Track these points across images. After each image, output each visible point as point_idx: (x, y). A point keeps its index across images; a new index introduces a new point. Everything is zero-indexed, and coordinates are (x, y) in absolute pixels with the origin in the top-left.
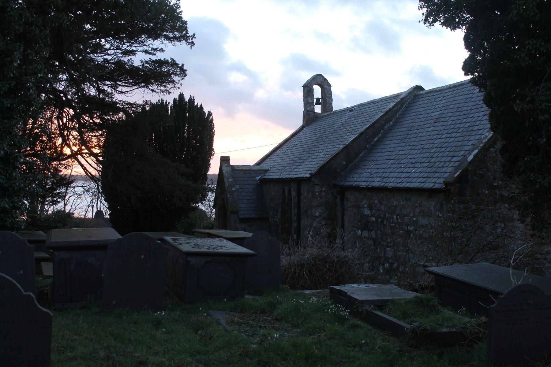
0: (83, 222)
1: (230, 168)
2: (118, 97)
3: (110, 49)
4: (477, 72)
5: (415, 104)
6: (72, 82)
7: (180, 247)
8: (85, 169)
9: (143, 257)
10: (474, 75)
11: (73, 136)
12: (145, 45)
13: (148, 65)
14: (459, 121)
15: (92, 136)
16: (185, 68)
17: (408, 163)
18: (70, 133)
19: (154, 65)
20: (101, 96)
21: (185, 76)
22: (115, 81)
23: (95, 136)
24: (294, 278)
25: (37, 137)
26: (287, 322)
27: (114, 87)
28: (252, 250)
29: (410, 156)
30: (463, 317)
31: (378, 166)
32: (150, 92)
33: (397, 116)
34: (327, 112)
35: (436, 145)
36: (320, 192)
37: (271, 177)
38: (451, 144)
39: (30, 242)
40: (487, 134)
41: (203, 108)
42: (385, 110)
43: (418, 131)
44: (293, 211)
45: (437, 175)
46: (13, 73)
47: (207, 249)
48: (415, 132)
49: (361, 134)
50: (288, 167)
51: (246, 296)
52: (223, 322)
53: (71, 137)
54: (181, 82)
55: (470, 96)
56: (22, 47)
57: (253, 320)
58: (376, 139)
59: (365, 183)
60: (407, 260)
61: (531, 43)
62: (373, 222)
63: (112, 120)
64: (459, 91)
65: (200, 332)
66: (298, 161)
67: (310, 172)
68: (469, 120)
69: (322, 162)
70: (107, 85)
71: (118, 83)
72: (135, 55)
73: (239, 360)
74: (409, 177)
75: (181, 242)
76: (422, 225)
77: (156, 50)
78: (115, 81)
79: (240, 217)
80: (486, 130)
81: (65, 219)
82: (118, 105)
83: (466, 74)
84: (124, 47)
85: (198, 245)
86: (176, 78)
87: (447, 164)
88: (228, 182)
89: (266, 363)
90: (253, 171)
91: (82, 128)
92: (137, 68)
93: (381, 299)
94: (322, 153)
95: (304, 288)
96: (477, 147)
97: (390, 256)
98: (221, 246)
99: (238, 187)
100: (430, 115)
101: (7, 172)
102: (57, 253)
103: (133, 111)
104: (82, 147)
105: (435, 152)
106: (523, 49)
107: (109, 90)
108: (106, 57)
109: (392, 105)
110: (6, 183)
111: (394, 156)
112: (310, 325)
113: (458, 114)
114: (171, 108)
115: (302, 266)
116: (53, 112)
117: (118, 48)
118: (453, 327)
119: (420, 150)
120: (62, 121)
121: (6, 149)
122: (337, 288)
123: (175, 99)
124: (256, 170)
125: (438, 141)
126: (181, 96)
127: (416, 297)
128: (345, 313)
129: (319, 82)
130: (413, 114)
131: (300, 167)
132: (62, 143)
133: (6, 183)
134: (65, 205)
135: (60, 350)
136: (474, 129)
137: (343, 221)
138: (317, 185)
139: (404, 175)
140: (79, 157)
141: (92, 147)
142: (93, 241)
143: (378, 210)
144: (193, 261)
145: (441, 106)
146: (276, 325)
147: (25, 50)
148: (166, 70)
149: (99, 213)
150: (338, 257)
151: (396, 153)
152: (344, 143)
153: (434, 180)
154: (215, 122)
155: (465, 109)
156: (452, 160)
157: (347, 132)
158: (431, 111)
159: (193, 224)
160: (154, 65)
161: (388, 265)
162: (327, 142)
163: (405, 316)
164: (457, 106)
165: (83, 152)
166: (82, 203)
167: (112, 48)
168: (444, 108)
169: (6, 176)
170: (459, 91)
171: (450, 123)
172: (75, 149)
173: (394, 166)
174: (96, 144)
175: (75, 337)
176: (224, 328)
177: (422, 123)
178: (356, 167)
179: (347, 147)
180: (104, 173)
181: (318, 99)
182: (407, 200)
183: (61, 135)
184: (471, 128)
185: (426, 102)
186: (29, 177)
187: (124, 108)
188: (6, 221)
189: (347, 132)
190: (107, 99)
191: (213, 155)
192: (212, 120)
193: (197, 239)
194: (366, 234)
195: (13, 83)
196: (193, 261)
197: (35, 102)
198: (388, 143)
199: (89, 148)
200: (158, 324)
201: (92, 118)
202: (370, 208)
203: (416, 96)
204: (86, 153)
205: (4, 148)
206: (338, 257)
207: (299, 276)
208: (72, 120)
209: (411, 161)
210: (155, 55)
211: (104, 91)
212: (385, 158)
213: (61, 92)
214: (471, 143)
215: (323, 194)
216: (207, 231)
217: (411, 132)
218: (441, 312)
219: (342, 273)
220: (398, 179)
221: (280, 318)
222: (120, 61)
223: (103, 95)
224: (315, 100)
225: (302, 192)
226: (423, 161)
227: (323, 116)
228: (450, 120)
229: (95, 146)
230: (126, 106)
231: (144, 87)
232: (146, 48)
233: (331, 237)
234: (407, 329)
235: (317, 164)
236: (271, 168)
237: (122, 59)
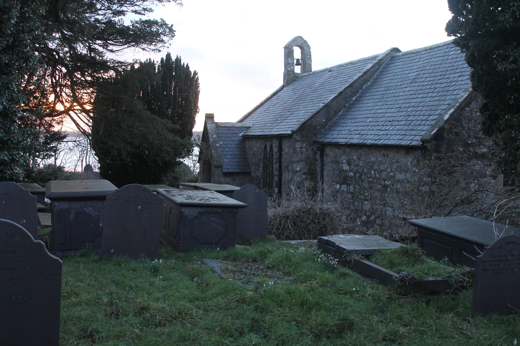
0: (72, 176)
1: (214, 125)
2: (108, 56)
3: (100, 9)
4: (459, 33)
5: (392, 65)
6: (64, 40)
8: (77, 125)
9: (140, 207)
10: (456, 36)
11: (65, 93)
12: (136, 5)
13: (138, 25)
14: (435, 82)
15: (83, 93)
16: (174, 28)
17: (386, 121)
18: (63, 90)
19: (143, 25)
20: (92, 55)
21: (173, 36)
22: (106, 40)
24: (279, 229)
25: (32, 93)
26: (278, 271)
29: (388, 115)
30: (447, 267)
31: (356, 124)
32: (141, 50)
33: (375, 76)
34: (306, 72)
35: (412, 105)
36: (301, 148)
37: (254, 134)
38: (427, 104)
39: (32, 193)
40: (462, 94)
41: (189, 68)
42: (364, 71)
43: (395, 91)
44: (274, 166)
45: (414, 133)
46: (11, 30)
47: (200, 200)
48: (392, 91)
49: (341, 93)
50: (269, 125)
51: (237, 246)
52: (218, 270)
53: (63, 94)
54: (170, 42)
55: (446, 58)
56: (19, 5)
57: (246, 268)
58: (354, 99)
59: (344, 140)
60: (383, 213)
61: (516, 4)
62: (351, 177)
63: (103, 78)
64: (435, 53)
65: (195, 279)
66: (279, 119)
67: (291, 129)
68: (444, 81)
69: (303, 119)
70: (98, 44)
72: (124, 15)
73: (237, 307)
74: (387, 135)
75: (174, 194)
76: (399, 180)
77: (145, 9)
78: (106, 40)
79: (224, 171)
80: (462, 91)
81: (56, 173)
82: (108, 64)
83: (449, 35)
85: (190, 197)
86: (165, 38)
87: (424, 122)
88: (212, 138)
89: (263, 309)
90: (235, 127)
91: (74, 85)
92: (128, 28)
93: (368, 249)
94: (303, 112)
95: (288, 238)
96: (453, 106)
97: (368, 210)
99: (221, 143)
100: (406, 75)
101: (6, 126)
102: (56, 204)
103: (123, 69)
104: (73, 103)
105: (412, 111)
106: (508, 11)
107: (101, 49)
108: (97, 17)
109: (370, 66)
110: (5, 136)
111: (372, 115)
112: (302, 273)
113: (434, 75)
114: (158, 67)
115: (287, 217)
116: (46, 70)
117: (109, 8)
118: (439, 276)
119: (398, 109)
120: (55, 79)
121: (4, 103)
122: (325, 238)
123: (162, 59)
124: (239, 127)
125: (414, 100)
126: (168, 56)
127: (402, 248)
128: (334, 262)
129: (299, 44)
130: (390, 75)
131: (282, 124)
132: (55, 100)
133: (5, 136)
134: (56, 159)
135: (65, 296)
136: (450, 89)
137: (322, 176)
138: (297, 141)
139: (382, 133)
140: (71, 113)
141: (84, 104)
142: (92, 192)
143: (357, 166)
144: (186, 211)
145: (417, 67)
146: (268, 273)
147: (22, 8)
148: (155, 30)
149: (88, 168)
150: (321, 209)
151: (373, 111)
152: (324, 102)
153: (411, 138)
155: (441, 70)
156: (428, 119)
157: (326, 91)
158: (408, 72)
159: (176, 176)
160: (143, 25)
161: (365, 217)
163: (391, 265)
164: (433, 67)
165: (75, 108)
166: (74, 157)
167: (103, 8)
168: (420, 69)
169: (5, 130)
170: (435, 53)
171: (426, 83)
172: (68, 105)
173: (373, 124)
174: (86, 101)
175: (78, 283)
176: (219, 276)
177: (399, 83)
178: (336, 124)
179: (327, 106)
180: (94, 128)
181: (298, 60)
182: (384, 156)
183: (55, 91)
184: (446, 89)
185: (403, 63)
186: (27, 131)
187: (114, 66)
188: (5, 173)
189: (326, 91)
190: (98, 58)
193: (189, 192)
194: (344, 188)
195: (11, 40)
196: (186, 211)
197: (32, 59)
198: (366, 102)
199: (81, 105)
200: (155, 271)
201: (83, 75)
202: (349, 163)
203: (393, 58)
204: (77, 110)
205: (3, 102)
206: (321, 209)
207: (284, 227)
208: (64, 76)
209: (389, 119)
210: (144, 15)
211: (94, 50)
212: (364, 116)
213: (54, 50)
214: (447, 102)
215: (304, 150)
216: (193, 184)
217: (388, 92)
218: (425, 261)
219: (324, 224)
220: (376, 136)
221: (271, 266)
222: (111, 21)
224: (295, 61)
225: (283, 148)
226: (400, 119)
227: (303, 77)
228: (426, 80)
229: (87, 103)
230: (116, 65)
231: (133, 46)
232: (136, 8)
233: (313, 192)
234: (396, 277)
235: (299, 121)
236: (253, 125)
237: (113, 19)
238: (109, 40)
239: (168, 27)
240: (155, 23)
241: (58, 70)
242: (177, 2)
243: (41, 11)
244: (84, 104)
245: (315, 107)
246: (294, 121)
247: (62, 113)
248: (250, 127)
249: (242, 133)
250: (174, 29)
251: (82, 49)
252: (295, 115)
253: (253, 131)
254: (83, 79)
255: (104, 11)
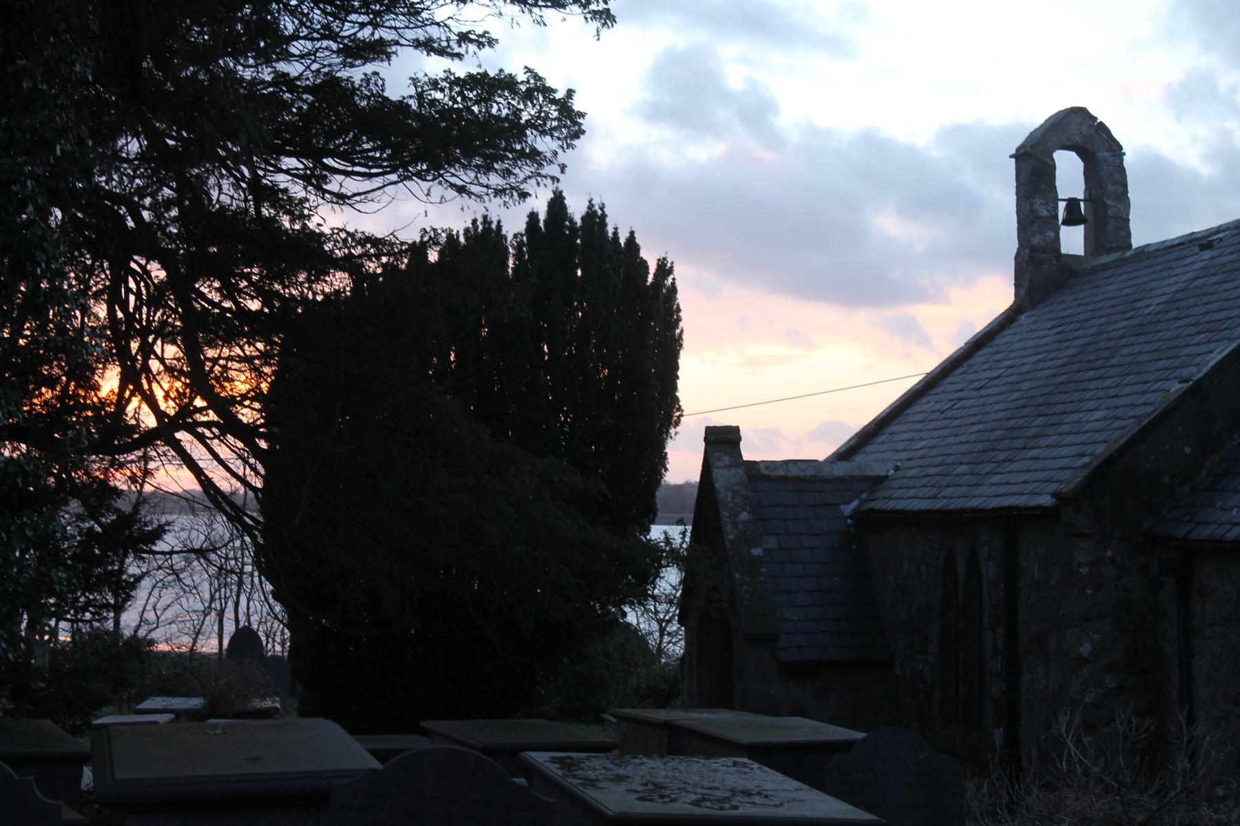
0: (184, 671)
2: (327, 218)
3: (294, 37)
6: (159, 161)
7: (592, 794)
13: (438, 95)
15: (229, 359)
16: (577, 105)
19: (461, 93)
20: (265, 212)
22: (316, 155)
23: (241, 359)
27: (316, 180)
28: (867, 808)
32: (452, 193)
34: (1109, 251)
37: (901, 505)
47: (697, 803)
50: (963, 468)
53: (155, 365)
67: (1053, 487)
69: (1101, 448)
70: (287, 172)
71: (329, 161)
75: (591, 774)
84: (348, 30)
85: (656, 790)
86: (545, 144)
88: (735, 524)
91: (198, 329)
92: (401, 106)
94: (1098, 415)
98: (747, 793)
99: (772, 542)
107: (297, 190)
108: (282, 67)
114: (519, 248)
116: (90, 271)
117: (329, 33)
120: (124, 308)
123: (533, 217)
124: (841, 479)
126: (557, 203)
129: (1077, 139)
131: (1013, 466)
148: (505, 112)
149: (245, 639)
152: (1185, 373)
154: (682, 299)
157: (1193, 330)
160: (461, 93)
162: (1114, 371)
179: (1197, 392)
183: (123, 356)
189: (1193, 330)
190: (287, 225)
191: (677, 423)
192: (673, 290)
197: (44, 251)
201: (229, 291)
204: (208, 425)
208: (155, 300)
211: (272, 195)
223: (272, 206)
224: (1062, 206)
227: (1094, 270)
229: (244, 397)
230: (358, 251)
231: (420, 175)
236: (897, 469)
237: (343, 74)
238: (333, 155)
239: (554, 102)
240: (506, 83)
241: (134, 273)
242: (593, 7)
243: (78, 68)
244: (232, 401)
245: (1150, 398)
246: (1065, 451)
247: (149, 438)
248: (886, 478)
249: (855, 504)
250: (576, 108)
251: (225, 193)
252: (1065, 428)
253: (899, 493)
254: (227, 304)
255: (309, 45)
